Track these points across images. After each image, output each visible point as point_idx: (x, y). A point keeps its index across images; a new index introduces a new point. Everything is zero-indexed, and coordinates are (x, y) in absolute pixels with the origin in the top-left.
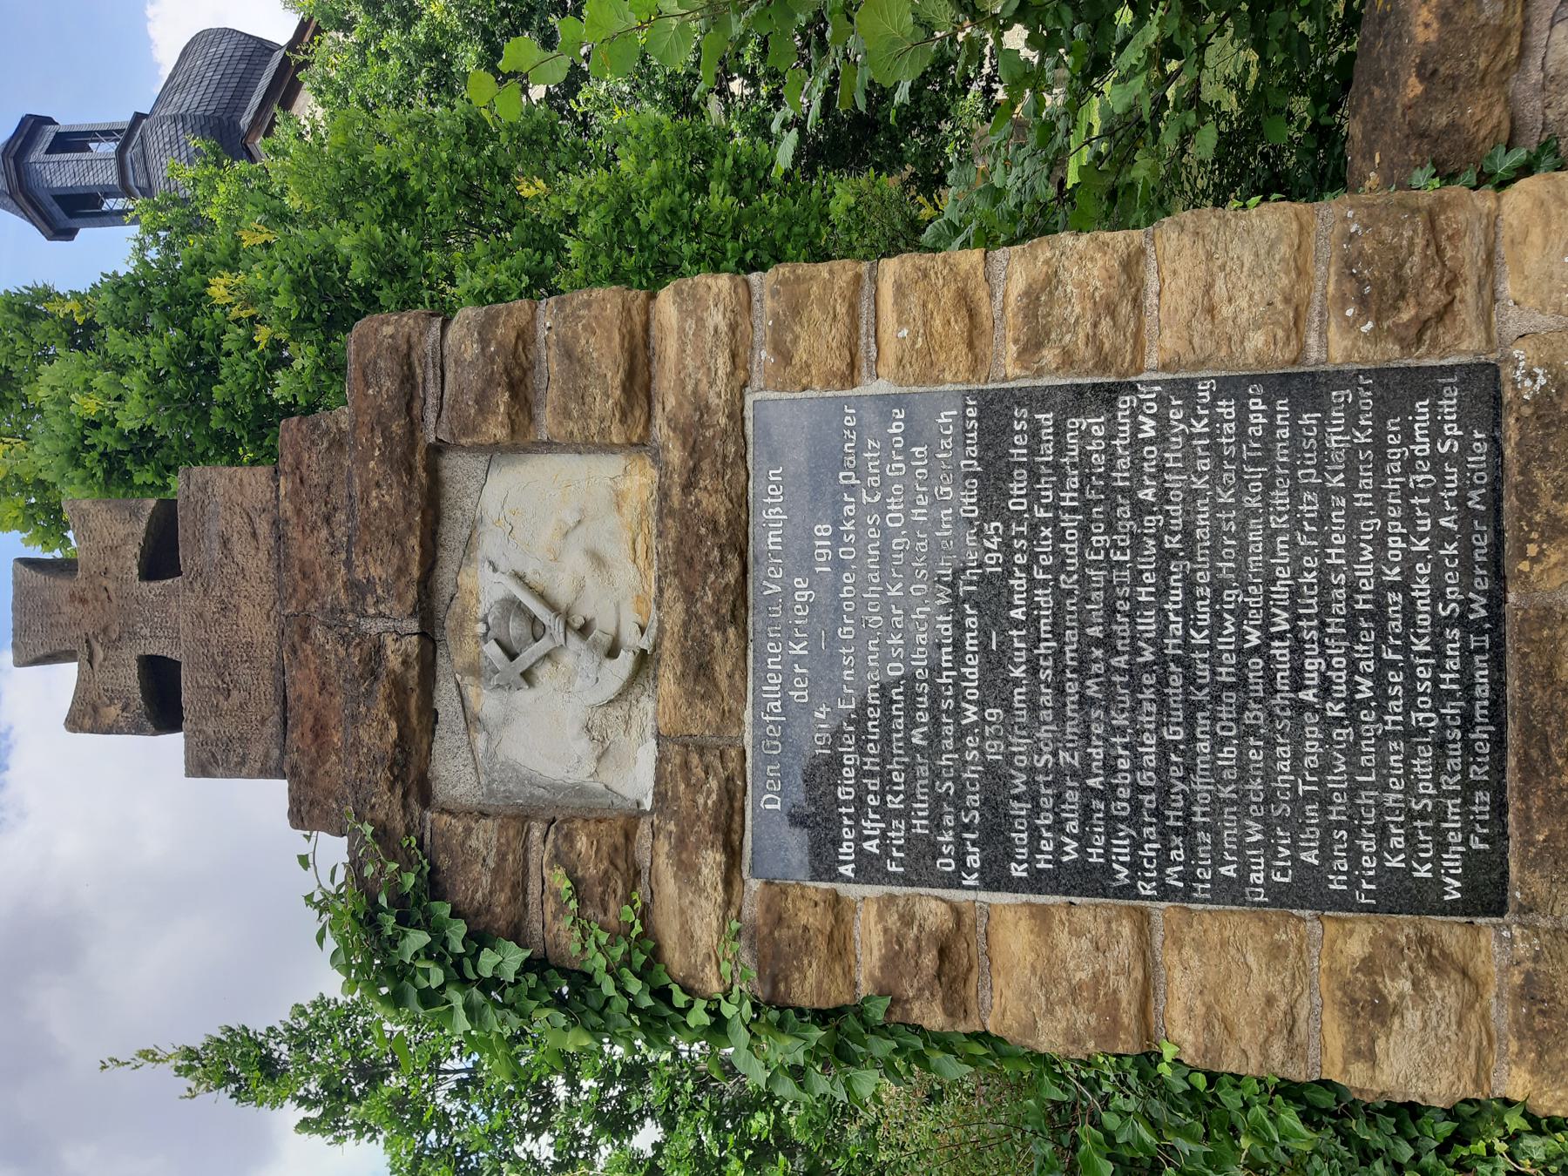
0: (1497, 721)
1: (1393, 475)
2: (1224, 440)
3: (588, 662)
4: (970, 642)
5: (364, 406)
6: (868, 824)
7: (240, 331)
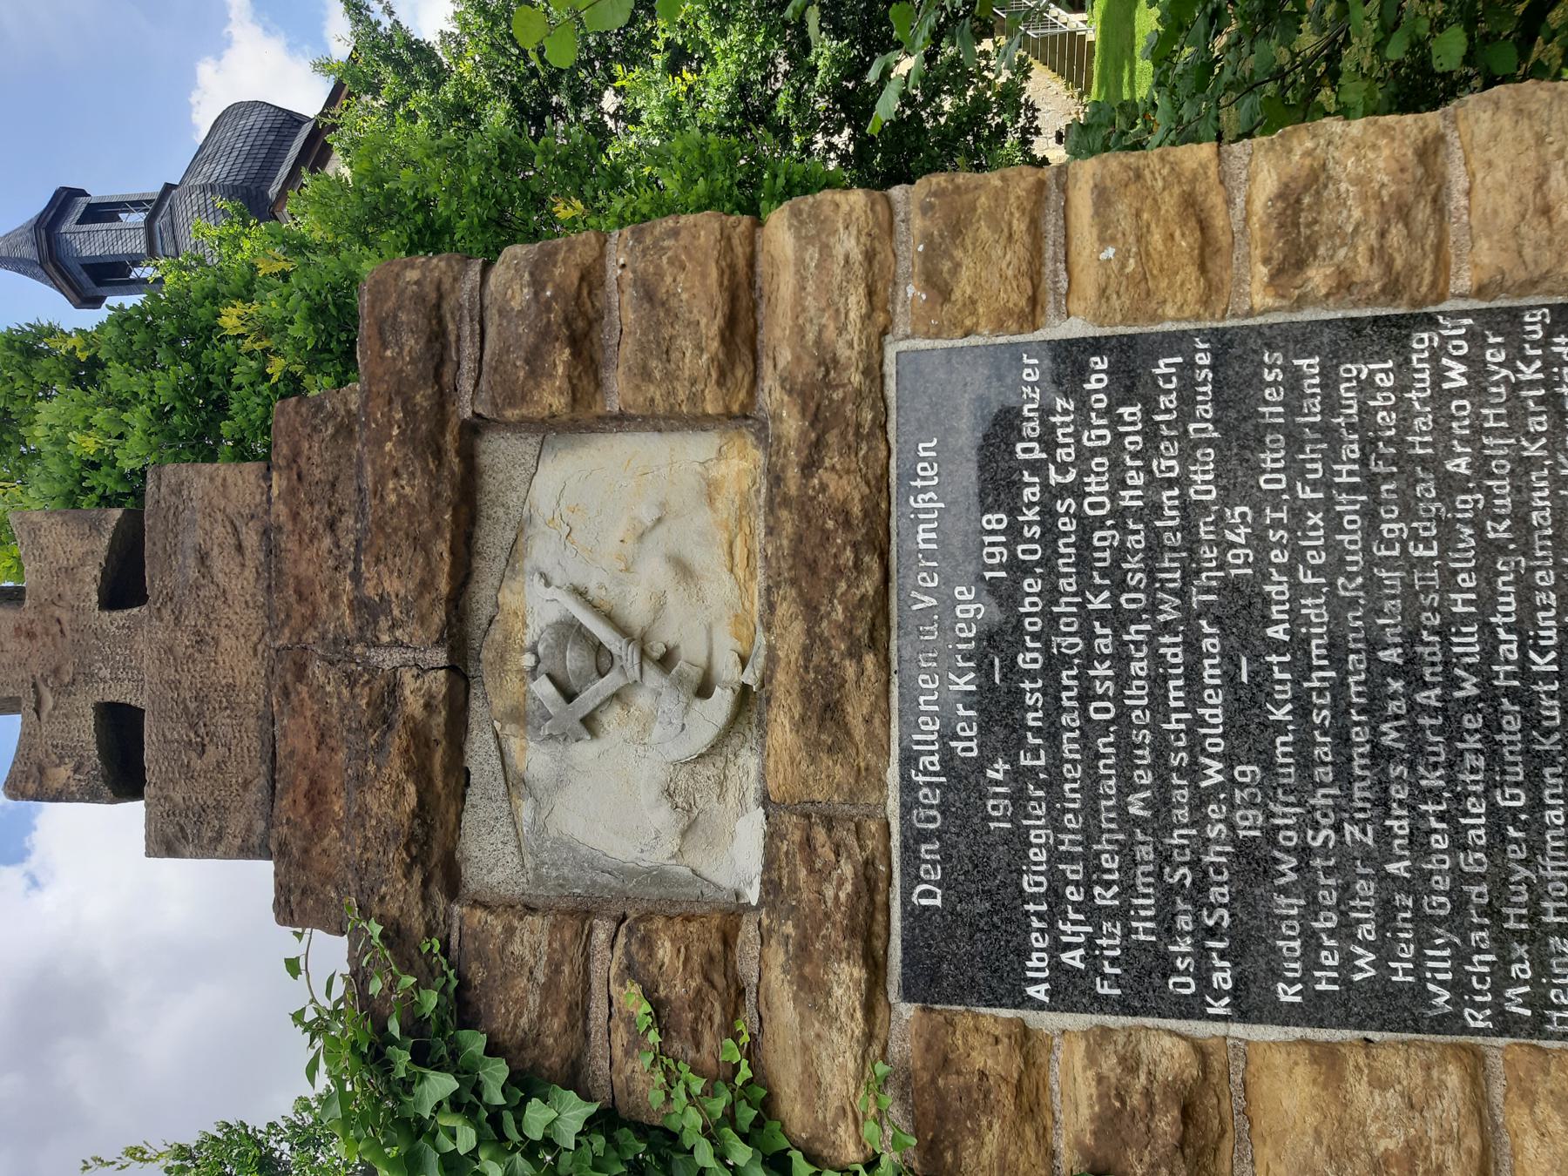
3: (671, 703)
4: (1210, 672)
5: (380, 371)
6: (1068, 928)
7: (252, 363)
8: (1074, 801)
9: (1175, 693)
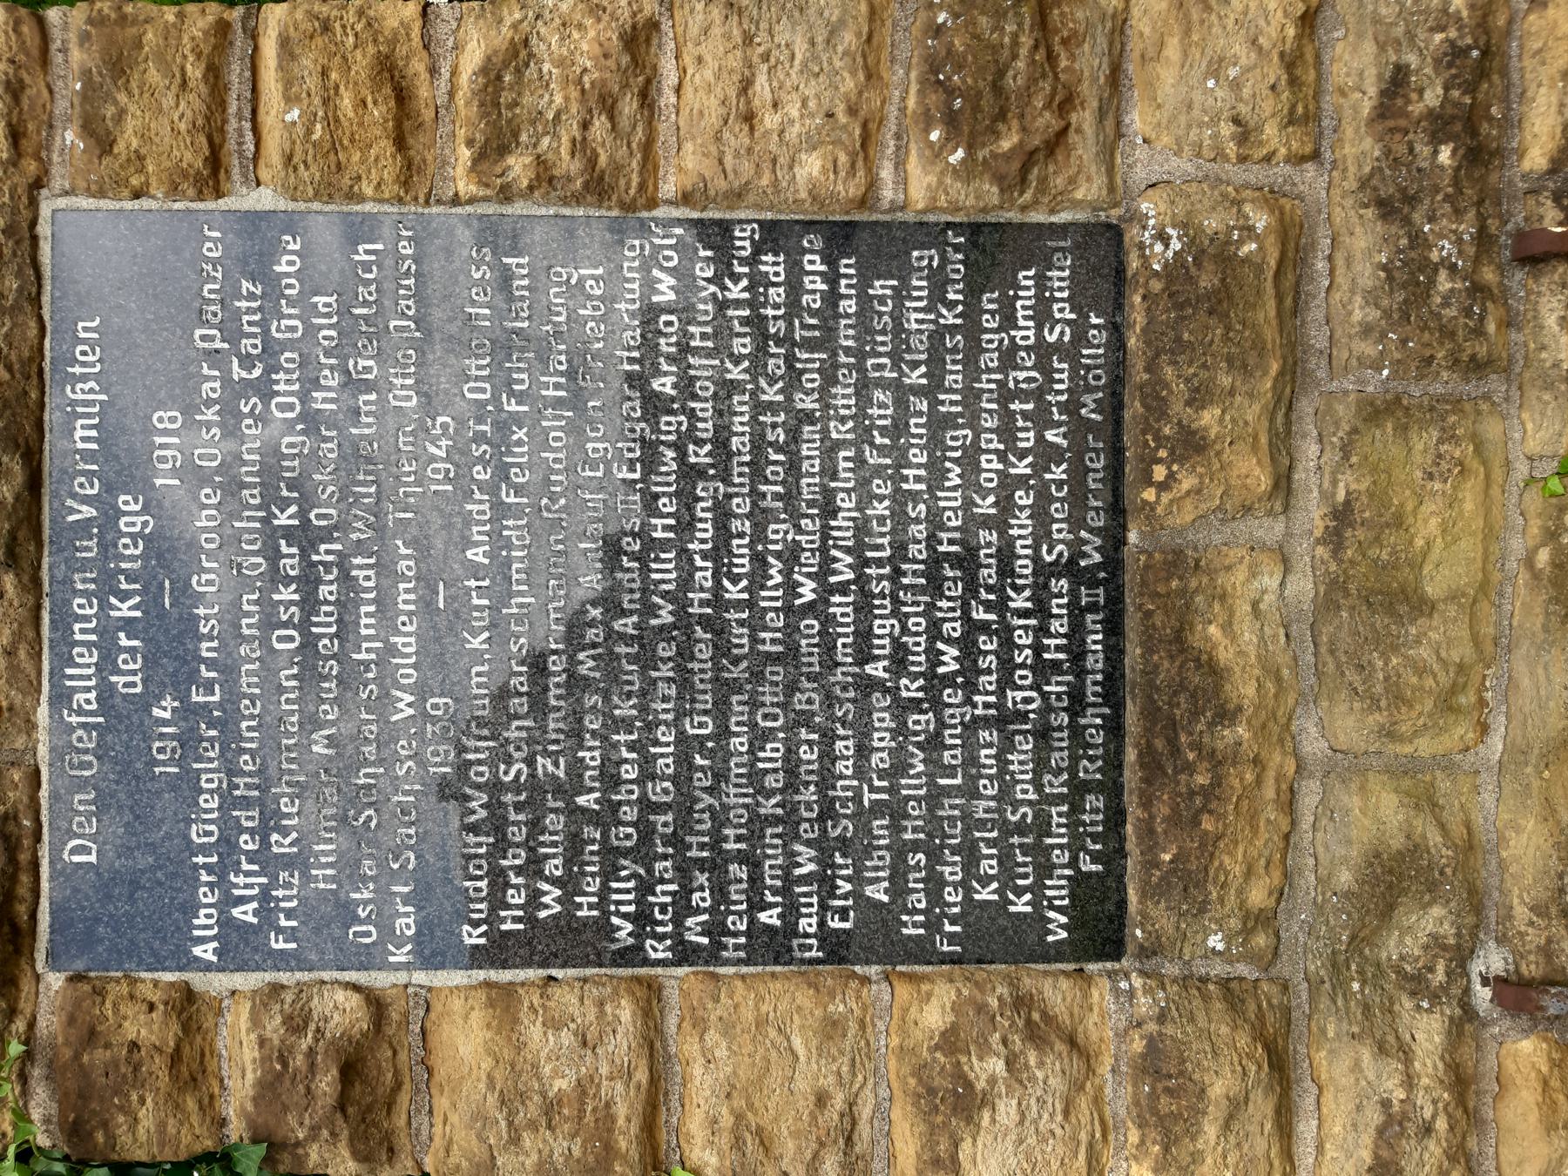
0: (1113, 700)
1: (989, 370)
2: (770, 312)
4: (405, 598)
6: (241, 880)
8: (252, 740)
9: (367, 624)
